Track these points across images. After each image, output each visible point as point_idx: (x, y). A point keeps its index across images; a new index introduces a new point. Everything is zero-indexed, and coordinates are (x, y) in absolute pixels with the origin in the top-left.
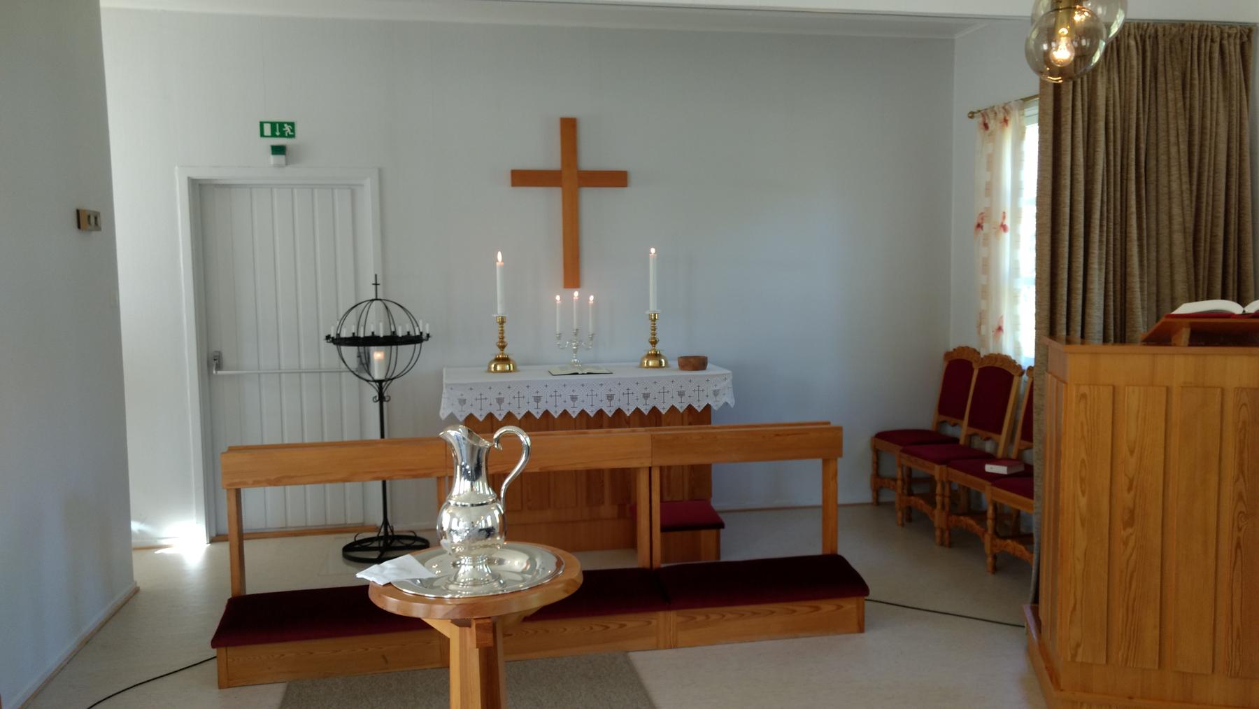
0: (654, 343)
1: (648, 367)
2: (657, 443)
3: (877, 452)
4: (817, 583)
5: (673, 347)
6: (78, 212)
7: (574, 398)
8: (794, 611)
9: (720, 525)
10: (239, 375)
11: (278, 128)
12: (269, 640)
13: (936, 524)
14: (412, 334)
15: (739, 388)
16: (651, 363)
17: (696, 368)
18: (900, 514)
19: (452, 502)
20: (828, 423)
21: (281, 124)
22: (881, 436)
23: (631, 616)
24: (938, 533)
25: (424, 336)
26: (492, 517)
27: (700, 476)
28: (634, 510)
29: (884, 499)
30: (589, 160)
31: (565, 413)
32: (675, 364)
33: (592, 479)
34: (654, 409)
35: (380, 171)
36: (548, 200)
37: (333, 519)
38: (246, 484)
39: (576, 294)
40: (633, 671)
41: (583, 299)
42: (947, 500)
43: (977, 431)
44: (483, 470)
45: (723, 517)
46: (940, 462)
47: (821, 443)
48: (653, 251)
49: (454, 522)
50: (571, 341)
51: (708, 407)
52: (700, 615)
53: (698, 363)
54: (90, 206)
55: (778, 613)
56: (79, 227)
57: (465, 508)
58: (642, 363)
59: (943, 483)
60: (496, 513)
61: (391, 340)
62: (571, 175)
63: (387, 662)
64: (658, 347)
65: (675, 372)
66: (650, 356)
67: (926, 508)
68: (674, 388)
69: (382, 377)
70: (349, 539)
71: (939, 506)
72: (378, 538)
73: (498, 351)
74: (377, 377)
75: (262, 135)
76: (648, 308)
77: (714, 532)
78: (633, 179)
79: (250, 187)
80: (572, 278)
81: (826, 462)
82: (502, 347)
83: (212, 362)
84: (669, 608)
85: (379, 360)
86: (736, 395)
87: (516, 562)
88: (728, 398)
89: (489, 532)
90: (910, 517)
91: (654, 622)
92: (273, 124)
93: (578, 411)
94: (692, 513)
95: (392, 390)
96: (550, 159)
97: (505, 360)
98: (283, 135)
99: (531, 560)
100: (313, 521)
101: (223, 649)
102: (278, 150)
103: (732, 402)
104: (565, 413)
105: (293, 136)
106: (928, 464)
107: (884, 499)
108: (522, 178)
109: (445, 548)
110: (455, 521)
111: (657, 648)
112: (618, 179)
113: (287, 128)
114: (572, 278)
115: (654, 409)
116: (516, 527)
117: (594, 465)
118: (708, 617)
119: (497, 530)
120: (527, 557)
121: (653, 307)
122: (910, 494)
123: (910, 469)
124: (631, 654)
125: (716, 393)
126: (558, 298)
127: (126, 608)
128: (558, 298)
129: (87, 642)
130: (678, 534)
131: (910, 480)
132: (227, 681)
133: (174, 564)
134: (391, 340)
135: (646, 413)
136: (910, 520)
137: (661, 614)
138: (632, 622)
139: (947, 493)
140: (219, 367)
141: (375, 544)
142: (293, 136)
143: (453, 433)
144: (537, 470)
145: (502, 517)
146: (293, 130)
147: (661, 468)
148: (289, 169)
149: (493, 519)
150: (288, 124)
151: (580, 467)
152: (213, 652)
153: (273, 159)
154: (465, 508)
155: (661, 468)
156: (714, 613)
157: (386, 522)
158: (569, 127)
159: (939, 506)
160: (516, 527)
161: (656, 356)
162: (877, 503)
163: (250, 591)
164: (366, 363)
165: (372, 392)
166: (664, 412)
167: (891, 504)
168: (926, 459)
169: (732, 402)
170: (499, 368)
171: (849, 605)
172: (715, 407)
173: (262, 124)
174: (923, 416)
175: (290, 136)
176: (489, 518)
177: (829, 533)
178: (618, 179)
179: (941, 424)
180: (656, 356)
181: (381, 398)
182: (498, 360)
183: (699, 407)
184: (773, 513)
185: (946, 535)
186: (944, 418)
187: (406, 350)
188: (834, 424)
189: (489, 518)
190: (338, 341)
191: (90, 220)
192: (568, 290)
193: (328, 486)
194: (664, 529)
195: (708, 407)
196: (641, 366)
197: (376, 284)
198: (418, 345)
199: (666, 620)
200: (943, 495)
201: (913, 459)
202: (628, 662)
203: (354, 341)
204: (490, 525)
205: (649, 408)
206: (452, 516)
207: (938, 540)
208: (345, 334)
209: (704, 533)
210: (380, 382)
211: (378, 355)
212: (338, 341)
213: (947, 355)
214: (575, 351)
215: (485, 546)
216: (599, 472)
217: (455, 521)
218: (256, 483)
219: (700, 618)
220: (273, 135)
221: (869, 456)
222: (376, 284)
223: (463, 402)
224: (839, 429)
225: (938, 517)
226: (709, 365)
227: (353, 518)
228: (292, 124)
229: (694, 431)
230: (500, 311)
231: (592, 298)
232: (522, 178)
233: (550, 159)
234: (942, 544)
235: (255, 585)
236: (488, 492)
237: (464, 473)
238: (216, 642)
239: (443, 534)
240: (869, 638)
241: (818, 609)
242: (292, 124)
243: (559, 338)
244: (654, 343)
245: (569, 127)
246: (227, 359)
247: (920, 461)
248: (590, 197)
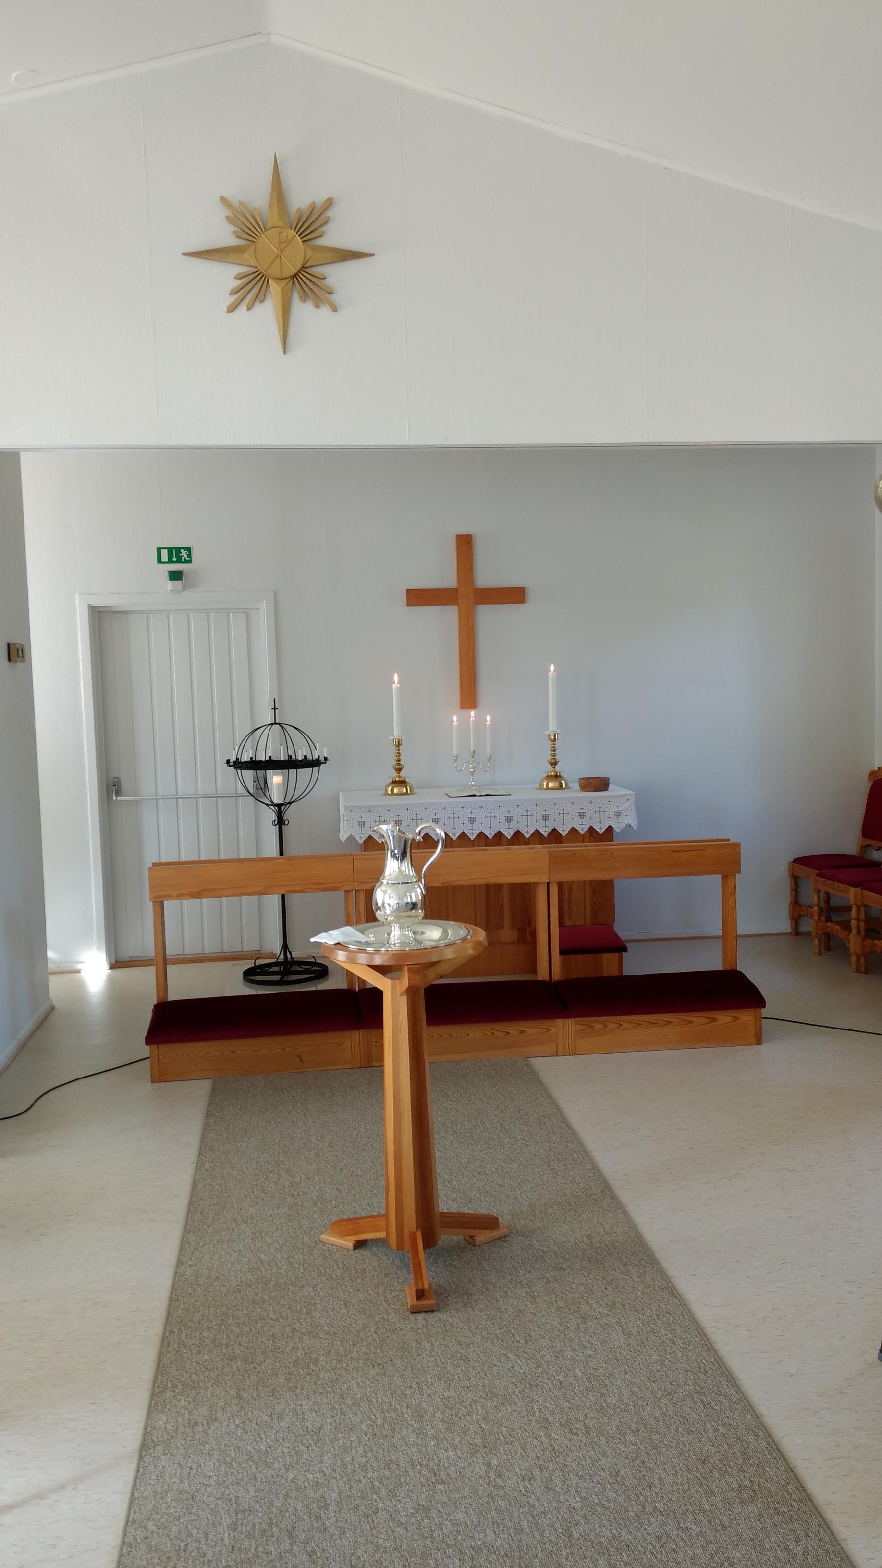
0: (554, 764)
1: (548, 789)
2: (553, 857)
3: (795, 879)
4: (719, 995)
5: (574, 768)
6: (9, 645)
7: (472, 820)
8: (691, 1022)
9: (624, 949)
10: (136, 801)
11: (177, 554)
12: (195, 1040)
13: (852, 950)
14: (309, 757)
15: (642, 806)
16: (551, 785)
17: (597, 789)
18: (816, 942)
19: (385, 882)
20: (728, 840)
21: (178, 550)
22: (799, 861)
23: (532, 1023)
24: (854, 959)
25: (322, 759)
26: (416, 894)
27: (602, 892)
28: (533, 934)
29: (802, 929)
30: (487, 576)
31: (463, 834)
32: (576, 786)
33: (492, 891)
34: (554, 830)
35: (276, 594)
36: (442, 620)
37: (229, 947)
38: (169, 897)
39: (473, 713)
40: (535, 1080)
41: (480, 721)
42: (862, 924)
43: (872, 842)
44: (408, 854)
45: (628, 945)
46: (855, 885)
47: (721, 859)
48: (552, 668)
49: (386, 898)
50: (468, 763)
51: (610, 829)
52: (598, 1022)
53: (600, 784)
54: (16, 640)
55: (674, 1023)
56: (10, 660)
57: (395, 886)
58: (541, 785)
59: (858, 907)
60: (419, 891)
61: (289, 764)
62: (468, 594)
63: (302, 1061)
64: (558, 768)
65: (575, 793)
66: (549, 778)
67: (842, 934)
68: (573, 812)
69: (282, 801)
70: (249, 964)
71: (854, 931)
72: (276, 964)
73: (395, 773)
74: (276, 801)
75: (159, 560)
76: (548, 729)
77: (617, 955)
78: (531, 595)
79: (147, 613)
80: (469, 697)
81: (725, 878)
82: (399, 770)
83: (111, 787)
84: (568, 1016)
85: (278, 784)
86: (639, 816)
87: (433, 933)
88: (631, 819)
89: (414, 906)
90: (829, 945)
91: (553, 1029)
92: (170, 550)
93: (476, 833)
94: (593, 932)
95: (290, 814)
96: (445, 576)
97: (402, 783)
98: (179, 560)
99: (445, 932)
100: (210, 947)
101: (155, 1047)
102: (175, 576)
103: (634, 824)
104: (463, 834)
105: (190, 561)
106: (843, 887)
107: (802, 929)
108: (417, 597)
109: (379, 918)
110: (387, 896)
111: (556, 1055)
112: (515, 595)
113: (184, 553)
114: (469, 697)
115: (554, 830)
116: (438, 903)
117: (493, 880)
118: (606, 1026)
119: (419, 906)
120: (441, 930)
121: (552, 727)
122: (828, 919)
123: (828, 895)
124: (532, 1061)
125: (618, 814)
126: (455, 718)
127: (44, 1023)
128: (455, 718)
129: (22, 1047)
130: (580, 957)
131: (829, 910)
132: (160, 1076)
133: (80, 986)
134: (289, 764)
135: (546, 835)
136: (828, 948)
137: (559, 1022)
138: (532, 1029)
139: (862, 916)
140: (118, 794)
141: (277, 969)
142: (190, 561)
143: (384, 827)
144: (439, 884)
145: (424, 896)
146: (189, 556)
147: (560, 885)
148: (185, 594)
149: (417, 895)
150: (185, 549)
151: (480, 882)
152: (145, 1050)
153: (170, 585)
154: (395, 886)
155: (560, 885)
156: (611, 1022)
157: (285, 947)
158: (465, 545)
159: (854, 931)
160: (438, 903)
161: (557, 777)
162: (796, 933)
163: (172, 997)
164: (263, 787)
165: (271, 815)
166: (564, 834)
167: (808, 934)
168: (839, 881)
169: (634, 824)
170: (396, 791)
171: (746, 1017)
172: (617, 829)
173: (159, 550)
174: (846, 839)
175: (186, 561)
176: (413, 895)
177: (729, 951)
178: (515, 595)
179: (865, 847)
180: (557, 777)
181: (281, 822)
182: (394, 782)
183: (600, 829)
184: (669, 925)
185: (862, 960)
186: (868, 841)
187: (305, 773)
188: (733, 840)
189: (413, 895)
190: (238, 765)
191: (17, 653)
192: (465, 711)
193: (244, 898)
194: (562, 952)
195: (610, 829)
196: (541, 788)
197: (275, 708)
198: (316, 769)
199: (565, 1028)
200: (858, 920)
201: (828, 882)
202: (529, 1065)
203: (253, 765)
204: (414, 900)
205: (549, 830)
206: (385, 892)
207: (854, 966)
208: (246, 758)
209: (606, 956)
210: (279, 805)
211: (276, 779)
212: (238, 765)
213: (872, 774)
214: (473, 773)
215: (410, 916)
216: (499, 887)
217: (387, 896)
218: (180, 896)
219: (598, 1026)
220: (170, 561)
221: (788, 883)
222: (275, 708)
223: (362, 824)
224: (738, 845)
225: (854, 943)
226: (611, 787)
227: (250, 945)
228: (188, 549)
229: (592, 847)
230: (397, 733)
231: (488, 718)
232: (417, 597)
233: (445, 576)
234: (858, 970)
235: (173, 995)
236: (412, 873)
237: (394, 856)
238: (149, 1040)
239: (379, 908)
240: (765, 1049)
241: (714, 1020)
242: (188, 549)
243: (456, 760)
244: (554, 764)
245: (465, 545)
246: (125, 784)
247: (836, 884)
248: (488, 616)
